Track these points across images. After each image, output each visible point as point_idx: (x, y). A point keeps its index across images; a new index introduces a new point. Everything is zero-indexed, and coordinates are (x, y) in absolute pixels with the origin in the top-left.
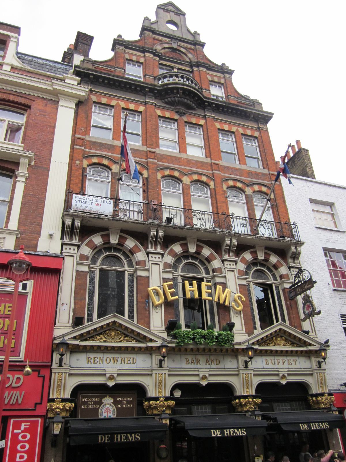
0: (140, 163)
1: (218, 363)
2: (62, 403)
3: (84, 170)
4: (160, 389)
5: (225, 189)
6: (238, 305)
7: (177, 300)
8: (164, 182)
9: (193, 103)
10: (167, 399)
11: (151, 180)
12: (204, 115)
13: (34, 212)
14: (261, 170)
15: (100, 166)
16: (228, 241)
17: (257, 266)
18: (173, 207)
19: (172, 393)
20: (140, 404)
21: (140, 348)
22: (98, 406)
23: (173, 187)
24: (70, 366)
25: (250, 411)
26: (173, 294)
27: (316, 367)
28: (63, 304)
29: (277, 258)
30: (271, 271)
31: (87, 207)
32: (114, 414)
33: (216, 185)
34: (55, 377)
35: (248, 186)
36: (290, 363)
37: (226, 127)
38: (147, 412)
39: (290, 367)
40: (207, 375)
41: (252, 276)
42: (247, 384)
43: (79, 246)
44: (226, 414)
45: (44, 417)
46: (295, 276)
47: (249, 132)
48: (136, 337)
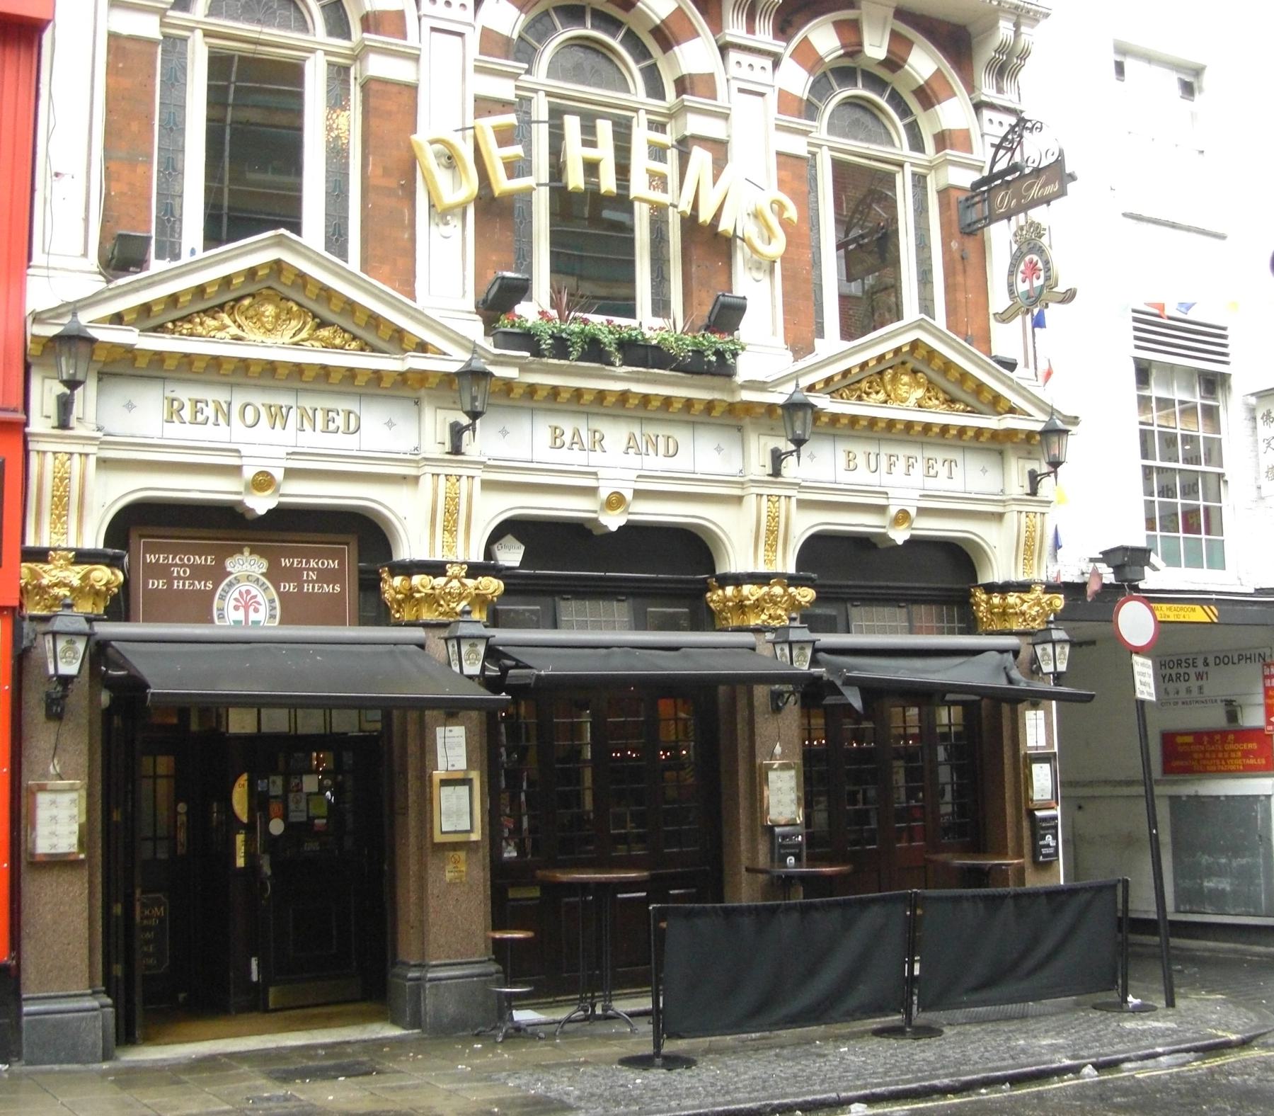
2: (78, 568)
4: (451, 532)
7: (527, 195)
10: (474, 571)
17: (584, 25)
19: (489, 554)
20: (369, 585)
21: (378, 375)
22: (210, 585)
24: (99, 430)
25: (774, 630)
27: (1021, 491)
28: (57, 175)
30: (904, 111)
32: (273, 617)
34: (43, 468)
36: (932, 472)
38: (397, 615)
46: (997, 141)
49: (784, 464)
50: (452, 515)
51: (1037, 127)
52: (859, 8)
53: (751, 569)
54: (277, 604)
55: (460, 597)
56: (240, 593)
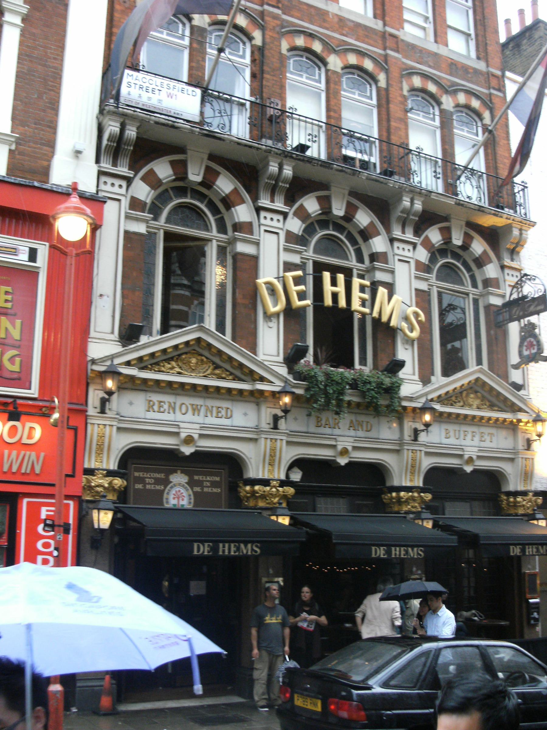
0: (436, 80)
1: (369, 428)
2: (107, 478)
5: (405, 93)
6: (412, 330)
8: (213, 37)
10: (283, 484)
11: (269, 55)
13: (40, 97)
16: (406, 203)
17: (186, 197)
18: (306, 117)
19: (287, 476)
20: (233, 489)
23: (308, 74)
24: (118, 414)
25: (413, 513)
26: (302, 296)
29: (370, 216)
30: (354, 242)
31: (149, 99)
32: (190, 503)
33: (390, 82)
34: (93, 431)
35: (447, 92)
36: (162, 410)
39: (483, 444)
40: (350, 448)
42: (413, 468)
43: (129, 181)
44: (309, 513)
45: (78, 499)
49: (419, 436)
50: (272, 457)
51: (532, 278)
52: (450, 222)
53: (260, 476)
54: (192, 497)
55: (274, 496)
56: (176, 492)
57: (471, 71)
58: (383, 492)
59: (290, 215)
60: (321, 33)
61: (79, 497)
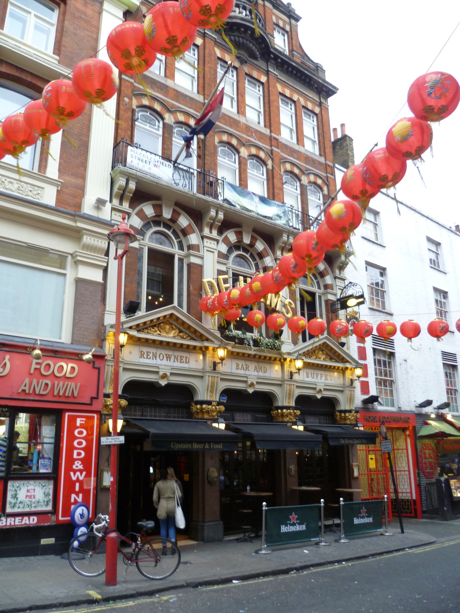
3: (133, 111)
9: (258, 51)
12: (203, 32)
14: (261, 128)
15: (149, 111)
16: (213, 213)
29: (324, 264)
30: (177, 236)
31: (144, 166)
37: (287, 93)
39: (327, 382)
41: (149, 238)
42: (290, 395)
47: (310, 106)
48: (190, 334)
52: (162, 201)
53: (205, 399)
57: (317, 162)
58: (272, 410)
59: (220, 242)
60: (236, 134)
61: (100, 412)
